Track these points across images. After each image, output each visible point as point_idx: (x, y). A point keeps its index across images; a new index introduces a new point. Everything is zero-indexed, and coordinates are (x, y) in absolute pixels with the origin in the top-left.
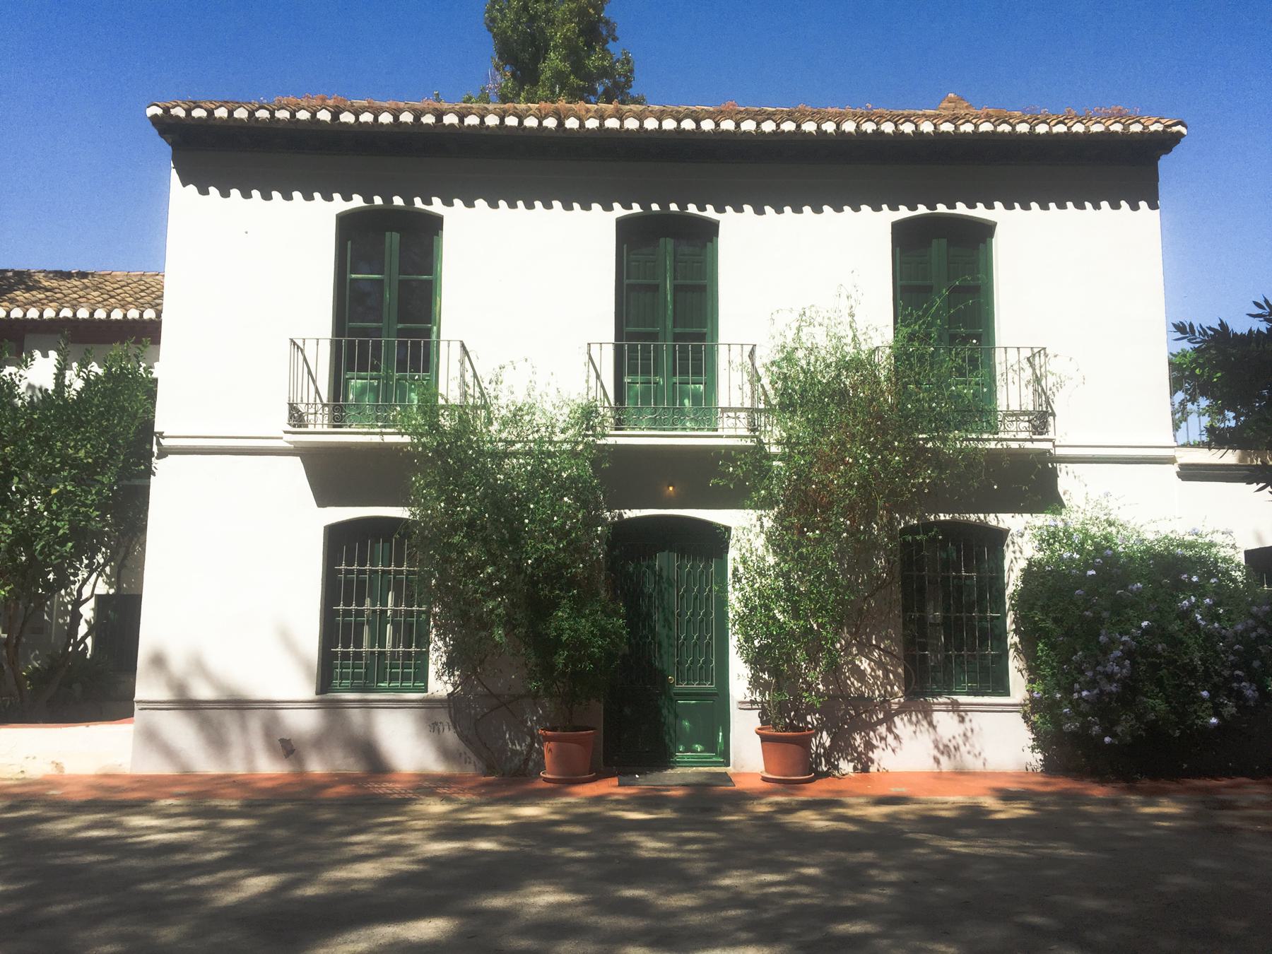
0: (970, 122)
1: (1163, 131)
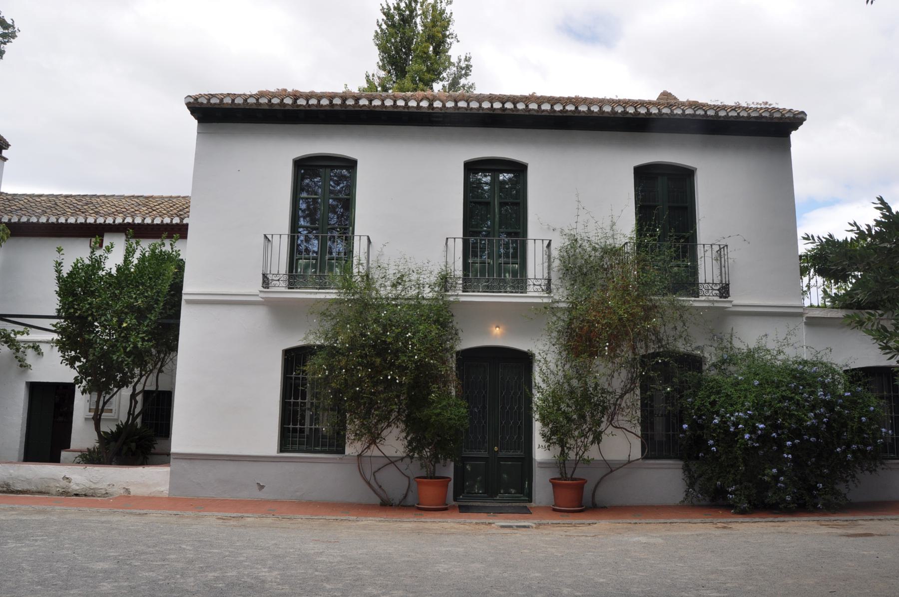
0: (680, 108)
1: (793, 117)
